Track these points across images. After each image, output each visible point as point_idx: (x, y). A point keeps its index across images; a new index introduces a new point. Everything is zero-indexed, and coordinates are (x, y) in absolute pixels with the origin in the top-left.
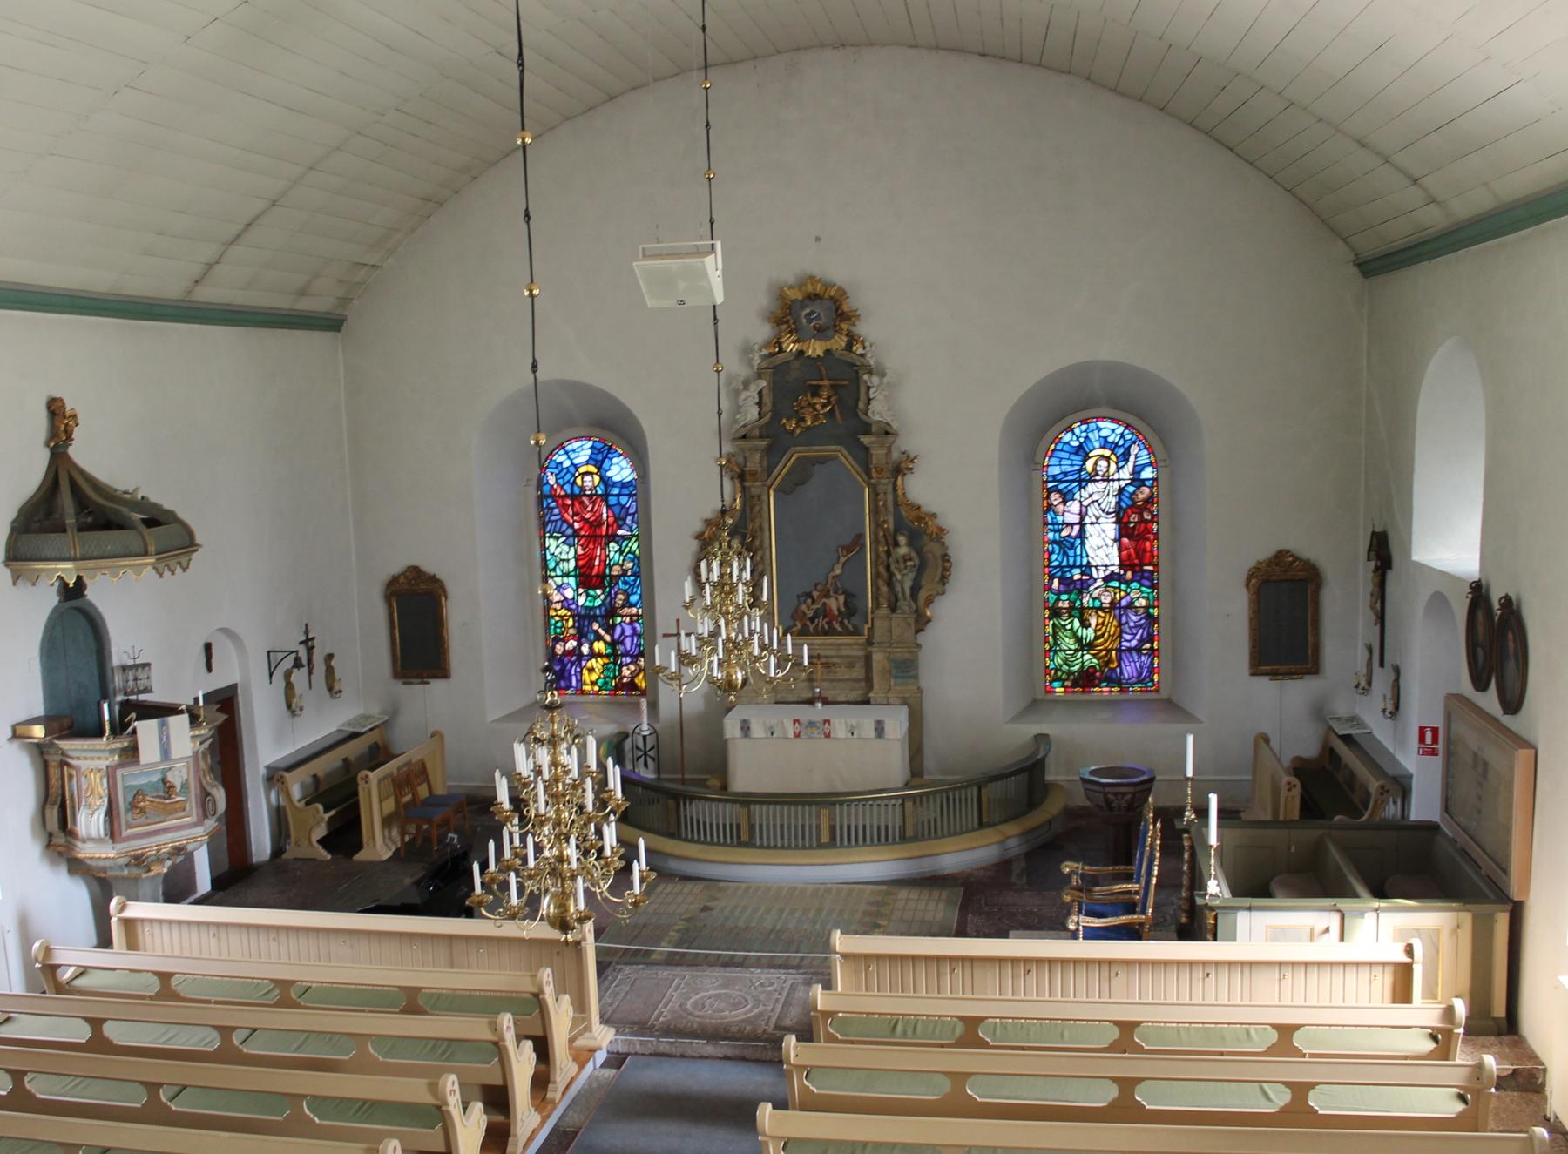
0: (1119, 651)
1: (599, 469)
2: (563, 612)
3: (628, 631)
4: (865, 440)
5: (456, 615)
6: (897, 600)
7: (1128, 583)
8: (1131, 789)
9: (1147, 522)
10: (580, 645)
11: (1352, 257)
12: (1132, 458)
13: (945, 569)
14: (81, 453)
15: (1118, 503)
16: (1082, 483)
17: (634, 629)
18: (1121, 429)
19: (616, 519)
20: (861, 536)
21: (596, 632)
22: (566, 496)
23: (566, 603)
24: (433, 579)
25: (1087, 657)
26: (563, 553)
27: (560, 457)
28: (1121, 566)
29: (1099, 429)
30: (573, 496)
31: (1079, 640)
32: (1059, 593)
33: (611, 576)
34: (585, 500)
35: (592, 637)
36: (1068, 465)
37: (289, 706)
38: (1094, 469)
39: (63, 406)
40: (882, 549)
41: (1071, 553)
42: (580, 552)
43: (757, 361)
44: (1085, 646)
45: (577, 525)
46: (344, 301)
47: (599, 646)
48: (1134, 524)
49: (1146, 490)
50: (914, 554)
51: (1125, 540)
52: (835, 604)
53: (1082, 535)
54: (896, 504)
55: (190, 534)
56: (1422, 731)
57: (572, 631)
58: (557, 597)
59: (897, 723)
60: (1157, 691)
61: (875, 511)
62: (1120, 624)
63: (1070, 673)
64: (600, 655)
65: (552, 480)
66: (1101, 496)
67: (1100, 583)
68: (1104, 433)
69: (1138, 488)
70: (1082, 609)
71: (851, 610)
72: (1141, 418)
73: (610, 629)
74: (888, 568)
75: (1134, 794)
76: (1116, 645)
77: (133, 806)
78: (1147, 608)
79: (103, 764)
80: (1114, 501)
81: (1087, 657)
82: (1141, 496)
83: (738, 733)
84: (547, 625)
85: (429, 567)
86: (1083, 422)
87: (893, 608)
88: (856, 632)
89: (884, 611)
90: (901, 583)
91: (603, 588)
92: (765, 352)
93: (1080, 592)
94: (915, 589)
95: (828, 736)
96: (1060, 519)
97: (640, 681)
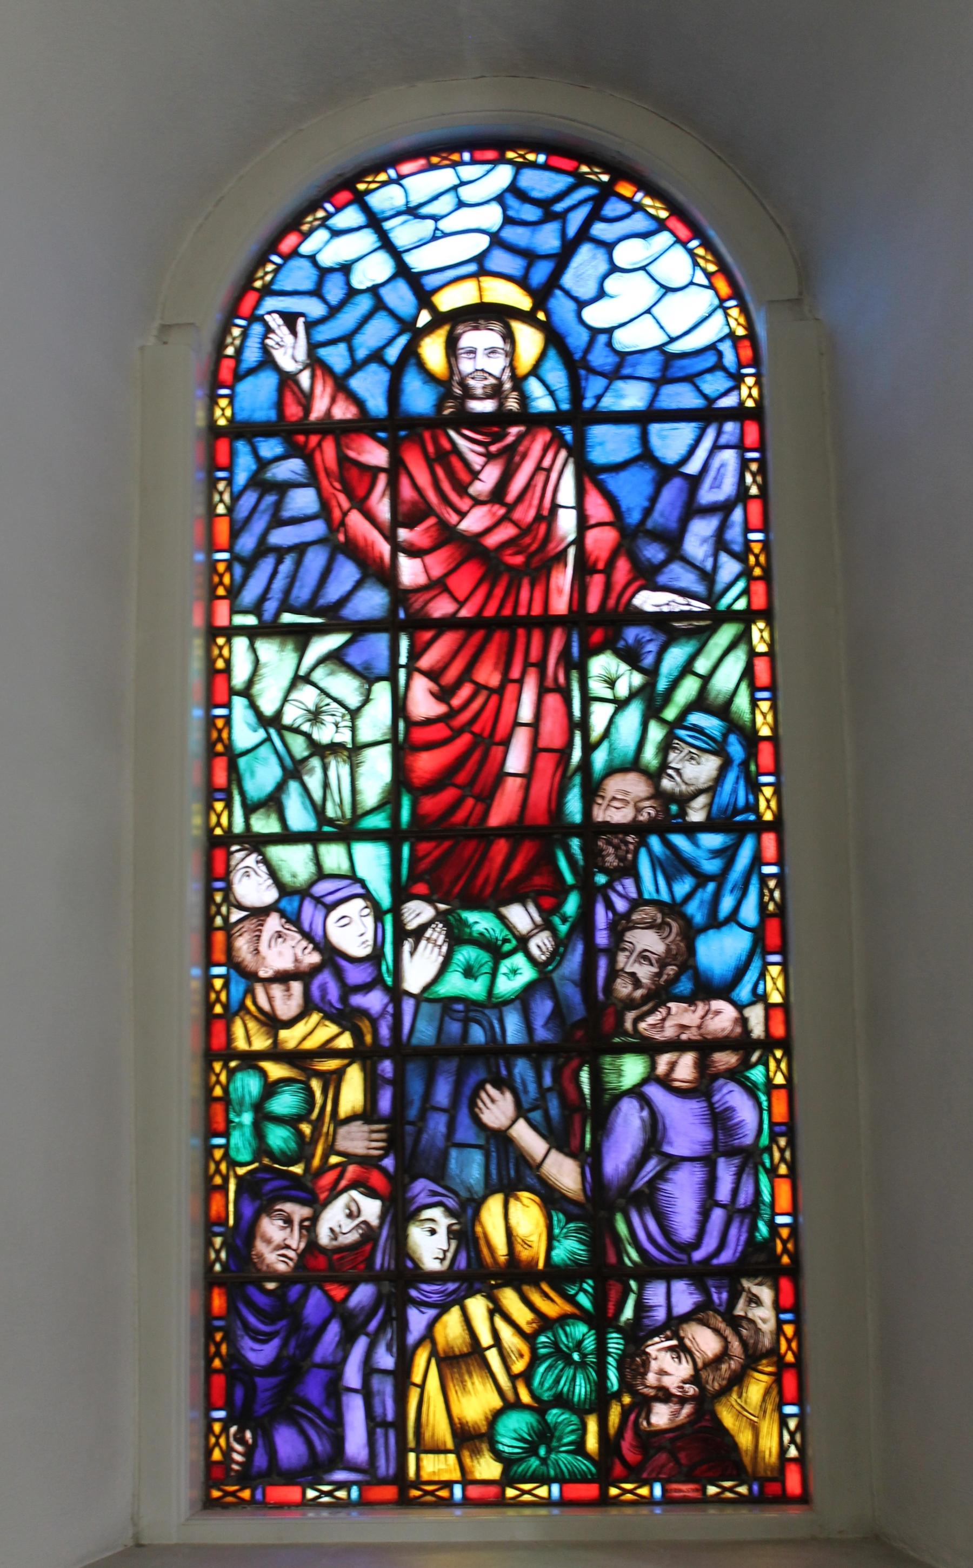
1: (541, 296)
3: (686, 1129)
10: (400, 1213)
17: (720, 1120)
19: (629, 535)
21: (500, 1141)
22: (365, 425)
26: (327, 714)
30: (397, 427)
33: (591, 830)
34: (467, 446)
35: (471, 1168)
42: (423, 703)
45: (410, 572)
47: (514, 1224)
56: (210, 1504)
64: (518, 1274)
65: (290, 352)
73: (579, 1122)
84: (214, 1114)
97: (755, 1422)
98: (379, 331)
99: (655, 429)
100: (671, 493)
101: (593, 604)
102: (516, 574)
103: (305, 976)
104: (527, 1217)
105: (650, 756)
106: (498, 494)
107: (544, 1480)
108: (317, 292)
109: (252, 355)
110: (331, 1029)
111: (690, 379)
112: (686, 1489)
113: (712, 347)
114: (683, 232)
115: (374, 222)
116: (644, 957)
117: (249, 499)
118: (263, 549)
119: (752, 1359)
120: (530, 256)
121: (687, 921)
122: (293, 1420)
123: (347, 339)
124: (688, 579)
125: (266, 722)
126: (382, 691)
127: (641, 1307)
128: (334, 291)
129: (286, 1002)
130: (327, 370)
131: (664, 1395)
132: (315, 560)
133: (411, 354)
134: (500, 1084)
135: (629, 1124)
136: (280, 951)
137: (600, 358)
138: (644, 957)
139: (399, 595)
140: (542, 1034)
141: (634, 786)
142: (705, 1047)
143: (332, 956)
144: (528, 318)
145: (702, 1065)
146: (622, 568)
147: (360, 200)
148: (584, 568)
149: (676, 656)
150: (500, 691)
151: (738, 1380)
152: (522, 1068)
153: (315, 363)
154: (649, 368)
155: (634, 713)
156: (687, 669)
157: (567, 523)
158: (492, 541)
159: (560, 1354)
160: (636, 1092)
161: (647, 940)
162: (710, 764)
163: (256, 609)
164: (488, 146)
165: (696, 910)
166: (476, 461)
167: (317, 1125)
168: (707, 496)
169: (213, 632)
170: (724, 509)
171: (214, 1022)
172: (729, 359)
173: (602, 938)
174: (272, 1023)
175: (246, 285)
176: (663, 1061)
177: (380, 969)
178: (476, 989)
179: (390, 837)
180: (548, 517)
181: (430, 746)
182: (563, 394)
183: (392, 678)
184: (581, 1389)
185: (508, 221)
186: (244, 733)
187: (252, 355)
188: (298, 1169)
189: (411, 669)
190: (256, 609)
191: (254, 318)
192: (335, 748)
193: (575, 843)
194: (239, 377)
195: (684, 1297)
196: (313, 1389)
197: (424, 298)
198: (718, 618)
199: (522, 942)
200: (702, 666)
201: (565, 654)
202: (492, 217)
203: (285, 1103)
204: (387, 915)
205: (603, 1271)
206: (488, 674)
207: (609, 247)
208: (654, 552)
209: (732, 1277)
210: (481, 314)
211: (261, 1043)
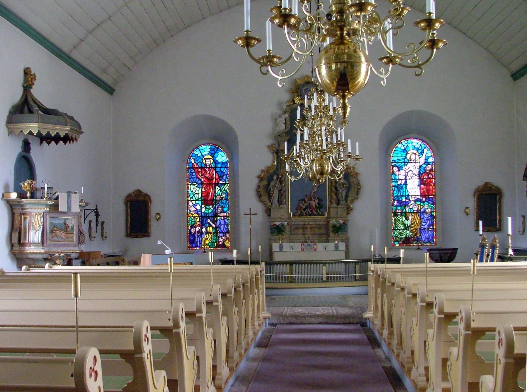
1: (213, 157)
2: (195, 215)
3: (223, 222)
5: (154, 209)
6: (339, 201)
7: (423, 202)
8: (450, 252)
9: (430, 178)
10: (202, 228)
11: (509, 73)
12: (424, 154)
13: (359, 189)
14: (36, 92)
15: (419, 171)
16: (405, 163)
17: (225, 222)
18: (420, 143)
19: (219, 177)
21: (209, 223)
22: (199, 168)
23: (197, 211)
24: (146, 195)
25: (408, 232)
27: (197, 152)
28: (421, 196)
29: (412, 143)
30: (201, 168)
31: (405, 225)
32: (397, 206)
33: (216, 200)
35: (207, 225)
37: (102, 236)
38: (410, 158)
39: (30, 71)
41: (401, 191)
42: (203, 190)
43: (285, 107)
44: (406, 228)
45: (202, 180)
46: (116, 82)
47: (210, 229)
48: (425, 179)
49: (430, 166)
50: (346, 182)
51: (422, 186)
52: (314, 203)
53: (405, 184)
55: (80, 128)
57: (199, 223)
58: (193, 209)
59: (342, 246)
60: (436, 245)
62: (421, 219)
63: (401, 238)
64: (210, 233)
65: (193, 161)
66: (413, 168)
67: (413, 202)
68: (414, 144)
69: (427, 165)
70: (406, 212)
71: (321, 206)
72: (427, 137)
73: (215, 222)
74: (336, 189)
75: (451, 253)
77: (52, 232)
79: (42, 211)
81: (408, 232)
82: (428, 169)
85: (144, 190)
87: (338, 203)
88: (323, 215)
89: (334, 205)
90: (341, 193)
91: (213, 205)
92: (287, 104)
93: (405, 206)
94: (347, 196)
95: (315, 250)
96: (397, 178)
97: (227, 244)
115: (200, 150)
129: (193, 213)
135: (218, 222)
136: (193, 209)
139: (202, 181)
141: (219, 197)
142: (224, 216)
157: (214, 176)
161: (220, 208)
164: (209, 144)
168: (225, 174)
174: (192, 214)
177: (200, 210)
179: (201, 200)
186: (190, 192)
195: (222, 235)
198: (226, 184)
202: (209, 150)
205: (216, 233)
210: (208, 158)
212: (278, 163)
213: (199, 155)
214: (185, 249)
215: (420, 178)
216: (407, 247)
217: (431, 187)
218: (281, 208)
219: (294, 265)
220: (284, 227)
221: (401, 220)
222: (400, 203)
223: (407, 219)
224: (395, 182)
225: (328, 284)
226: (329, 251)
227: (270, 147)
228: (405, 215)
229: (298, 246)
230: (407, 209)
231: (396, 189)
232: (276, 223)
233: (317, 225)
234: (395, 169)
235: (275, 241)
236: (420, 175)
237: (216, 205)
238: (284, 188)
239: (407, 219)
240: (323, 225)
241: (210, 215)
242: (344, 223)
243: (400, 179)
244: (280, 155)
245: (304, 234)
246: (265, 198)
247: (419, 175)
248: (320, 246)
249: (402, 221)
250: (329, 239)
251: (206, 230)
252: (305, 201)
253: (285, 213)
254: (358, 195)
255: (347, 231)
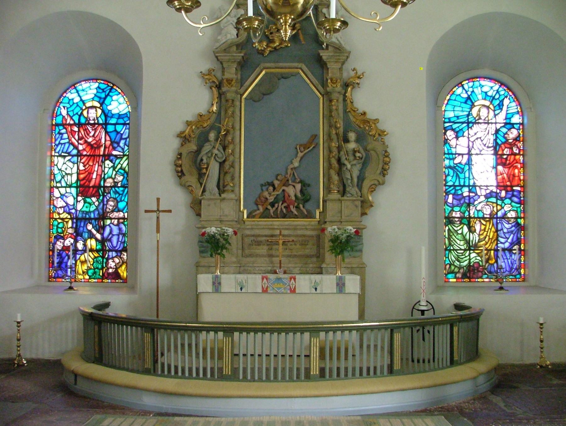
0: (496, 250)
1: (102, 104)
2: (65, 215)
3: (116, 231)
4: (324, 55)
9: (515, 154)
10: (76, 241)
12: (505, 108)
13: (386, 163)
15: (495, 140)
17: (120, 229)
18: (496, 87)
19: (112, 142)
20: (315, 137)
21: (90, 232)
22: (75, 124)
26: (67, 169)
28: (498, 187)
30: (79, 125)
31: (468, 242)
32: (453, 206)
33: (104, 187)
35: (86, 235)
36: (461, 111)
38: (478, 115)
40: (334, 144)
41: (462, 176)
42: (82, 167)
44: (471, 247)
45: (81, 148)
47: (92, 243)
51: (500, 168)
52: (292, 191)
53: (469, 163)
54: (345, 112)
56: (49, 281)
58: (60, 203)
59: (353, 283)
60: (524, 280)
61: (329, 115)
62: (497, 231)
63: (460, 268)
64: (91, 250)
65: (64, 112)
66: (483, 134)
67: (482, 198)
68: (485, 89)
69: (509, 129)
70: (470, 217)
71: (305, 197)
73: (101, 229)
74: (339, 160)
76: (494, 246)
78: (516, 218)
80: (492, 138)
81: (473, 255)
83: (210, 288)
84: (51, 227)
86: (470, 79)
87: (344, 192)
88: (310, 215)
89: (335, 195)
93: (469, 205)
95: (293, 291)
96: (453, 151)
97: (123, 272)
98: (78, 110)
99: (117, 126)
100: (119, 136)
101: (106, 153)
102: (95, 148)
103: (64, 207)
104: (93, 242)
105: (113, 176)
106: (93, 136)
107: (94, 279)
108: (69, 103)
109: (59, 113)
110: (67, 215)
111: (123, 118)
112: (113, 281)
113: (126, 113)
114: (123, 94)
115: (77, 92)
116: (111, 206)
117: (58, 136)
118: (59, 143)
119: (123, 263)
120: (100, 98)
121: (117, 201)
122: (61, 270)
123: (73, 111)
124: (120, 149)
125: (59, 170)
126: (76, 165)
127: (108, 255)
128: (71, 103)
129: (61, 211)
130: (70, 116)
131: (111, 268)
132: (67, 145)
133: (82, 113)
134: (90, 223)
135: (108, 230)
137: (110, 115)
138: (111, 206)
139: (79, 151)
140: (96, 216)
141: (111, 180)
142: (119, 219)
143: (67, 204)
144: (99, 108)
145: (118, 221)
146: (111, 147)
147: (75, 88)
148: (105, 147)
149: (118, 161)
150: (92, 166)
151: (121, 266)
152: (93, 221)
153: (68, 114)
154: (117, 117)
155: (112, 169)
156: (119, 163)
157: (103, 141)
158: (92, 143)
159: (97, 262)
160: (109, 225)
161: (111, 203)
162: (122, 177)
163: (58, 153)
164: (96, 80)
165: (118, 199)
166: (91, 130)
167: (65, 229)
168: (124, 137)
169: (52, 156)
170: (126, 139)
171: (51, 213)
172: (128, 115)
173: (105, 203)
174: (59, 214)
175: (58, 101)
176: (113, 220)
178: (87, 210)
180: (100, 140)
181: (82, 174)
182: (104, 120)
183: (77, 164)
184: (100, 267)
185: (97, 92)
186: (56, 171)
187: (59, 113)
188: (62, 235)
189: (80, 162)
190: (58, 153)
191: (59, 107)
192: (69, 174)
193: (102, 189)
194: (56, 116)
195: (114, 254)
196: (64, 266)
197: (84, 104)
198: (124, 155)
199: (94, 203)
200: (121, 163)
201: (102, 161)
202: (95, 91)
203: (61, 225)
204: (76, 199)
205: (103, 250)
206: (91, 163)
207: (112, 97)
208: (115, 145)
209: (121, 251)
211: (58, 217)
212: (220, 108)
213: (75, 101)
214: (44, 280)
215: (496, 153)
216: (470, 284)
217: (516, 171)
218: (224, 199)
219: (236, 334)
220: (226, 240)
221: (460, 232)
222: (460, 200)
223: (471, 230)
224: (450, 159)
225: (324, 387)
226: (322, 297)
227: (206, 76)
228: (468, 221)
229: (254, 281)
230: (472, 212)
231: (451, 172)
232: (208, 230)
233: (297, 236)
234: (450, 134)
235: (208, 269)
236: (496, 147)
237: (104, 196)
238: (231, 158)
239: (471, 230)
240: (312, 236)
241: (92, 216)
242: (357, 232)
243: (459, 154)
244: (224, 89)
245: (271, 256)
246: (192, 179)
247: (495, 148)
248: (304, 282)
249: (462, 234)
250: (324, 266)
251: (85, 245)
252: (273, 186)
253: (230, 211)
254: (384, 175)
255: (361, 251)
